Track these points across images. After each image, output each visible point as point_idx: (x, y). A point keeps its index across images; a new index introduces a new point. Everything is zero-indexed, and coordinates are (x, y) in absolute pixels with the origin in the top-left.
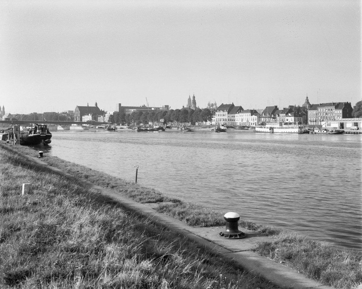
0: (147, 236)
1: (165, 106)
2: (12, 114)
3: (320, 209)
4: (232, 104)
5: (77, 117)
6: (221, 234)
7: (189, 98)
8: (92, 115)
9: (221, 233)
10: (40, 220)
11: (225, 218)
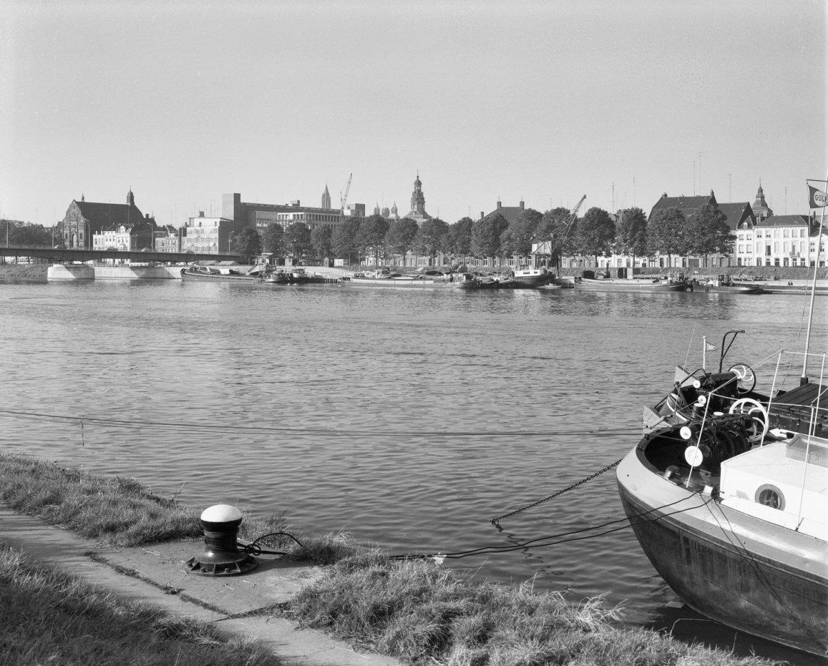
4: (709, 194)
5: (75, 237)
6: (194, 564)
7: (323, 191)
8: (130, 230)
9: (192, 560)
10: (159, 640)
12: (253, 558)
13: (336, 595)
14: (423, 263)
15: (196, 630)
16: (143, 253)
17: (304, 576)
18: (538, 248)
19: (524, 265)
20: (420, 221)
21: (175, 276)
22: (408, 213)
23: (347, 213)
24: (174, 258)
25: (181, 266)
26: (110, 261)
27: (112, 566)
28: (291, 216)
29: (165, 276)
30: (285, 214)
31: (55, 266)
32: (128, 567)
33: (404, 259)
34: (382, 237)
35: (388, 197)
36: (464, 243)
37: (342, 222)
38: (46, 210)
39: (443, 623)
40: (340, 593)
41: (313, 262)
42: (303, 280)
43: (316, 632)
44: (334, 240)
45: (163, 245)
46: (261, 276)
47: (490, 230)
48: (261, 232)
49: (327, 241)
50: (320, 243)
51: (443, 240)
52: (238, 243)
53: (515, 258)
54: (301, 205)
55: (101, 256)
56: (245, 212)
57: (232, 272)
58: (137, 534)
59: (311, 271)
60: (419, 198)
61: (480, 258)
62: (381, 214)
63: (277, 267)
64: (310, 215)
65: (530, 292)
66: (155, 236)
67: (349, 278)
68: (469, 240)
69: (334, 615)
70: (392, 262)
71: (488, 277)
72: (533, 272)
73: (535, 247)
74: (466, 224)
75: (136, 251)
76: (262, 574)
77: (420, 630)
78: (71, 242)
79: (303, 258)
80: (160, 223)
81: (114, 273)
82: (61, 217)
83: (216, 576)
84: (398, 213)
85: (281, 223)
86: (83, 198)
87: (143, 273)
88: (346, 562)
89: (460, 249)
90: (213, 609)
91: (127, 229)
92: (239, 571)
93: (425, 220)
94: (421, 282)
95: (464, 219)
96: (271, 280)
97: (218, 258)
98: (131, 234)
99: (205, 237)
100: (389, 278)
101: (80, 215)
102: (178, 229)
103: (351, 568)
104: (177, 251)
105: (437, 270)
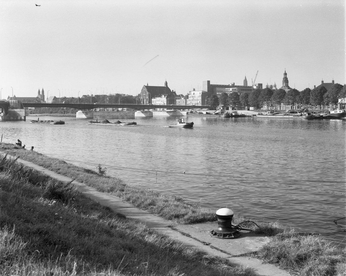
1: (258, 84)
2: (57, 97)
3: (223, 197)
5: (145, 100)
7: (244, 79)
8: (166, 96)
9: (213, 231)
12: (238, 231)
13: (279, 250)
14: (288, 108)
15: (221, 261)
16: (171, 106)
17: (262, 240)
18: (341, 101)
19: (335, 109)
20: (287, 90)
21: (184, 115)
22: (281, 87)
23: (255, 87)
24: (184, 108)
25: (187, 111)
26: (158, 109)
27: (180, 232)
28: (231, 89)
29: (180, 115)
30: (228, 88)
31: (138, 111)
32: (186, 233)
33: (280, 107)
34: (270, 98)
35: (273, 80)
36: (307, 99)
37: (253, 92)
38: (133, 89)
39: (331, 265)
40: (281, 249)
41: (241, 109)
42: (237, 116)
43: (271, 265)
44: (250, 99)
45: (179, 102)
46: (219, 115)
47: (318, 93)
48: (219, 96)
49: (247, 99)
50: (244, 100)
51: (297, 98)
52: (209, 101)
53: (330, 105)
54: (235, 85)
55: (155, 107)
56: (212, 88)
57: (207, 113)
58: (188, 219)
59: (240, 112)
60: (286, 80)
61: (314, 106)
62: (269, 87)
63: (226, 111)
64: (240, 89)
65: (338, 121)
66: (176, 99)
67: (256, 115)
68: (309, 98)
69: (279, 258)
70: (275, 108)
71: (318, 114)
72: (339, 111)
73: (340, 100)
74: (308, 91)
75: (169, 105)
76: (243, 238)
77: (321, 267)
78: (144, 102)
79: (237, 107)
80: (178, 94)
81: (159, 114)
82: (139, 92)
83: (223, 238)
84: (276, 87)
85: (227, 93)
86: (148, 84)
87: (171, 114)
88: (280, 235)
89: (305, 102)
90: (225, 252)
91: (165, 96)
92: (233, 237)
93: (289, 90)
94: (288, 116)
95: (307, 89)
96: (223, 116)
97: (201, 107)
98: (167, 98)
99: (196, 99)
100: (273, 115)
102: (185, 96)
103: (283, 238)
104: (185, 105)
105: (295, 111)
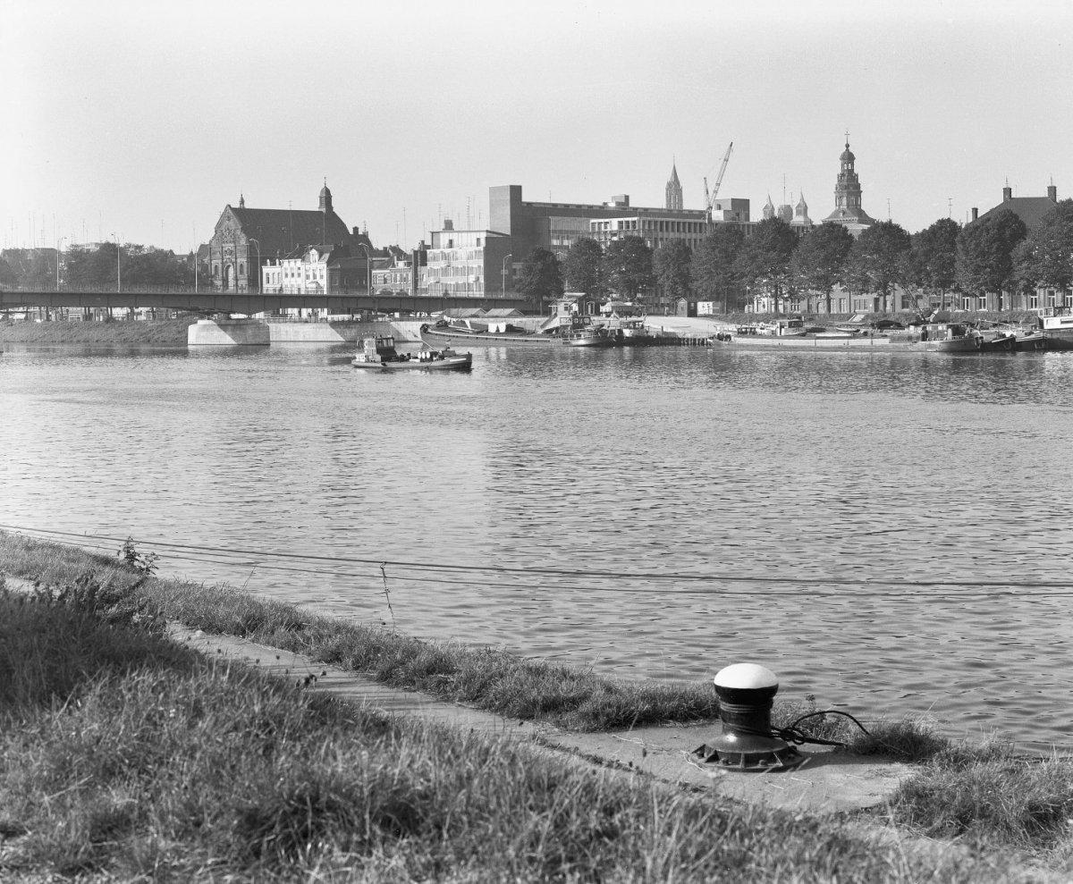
0: (344, 644)
5: (231, 271)
7: (668, 177)
8: (327, 256)
11: (718, 689)
98: (329, 263)
101: (239, 232)
